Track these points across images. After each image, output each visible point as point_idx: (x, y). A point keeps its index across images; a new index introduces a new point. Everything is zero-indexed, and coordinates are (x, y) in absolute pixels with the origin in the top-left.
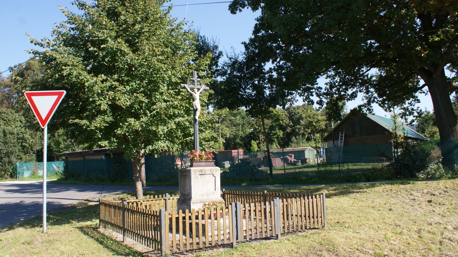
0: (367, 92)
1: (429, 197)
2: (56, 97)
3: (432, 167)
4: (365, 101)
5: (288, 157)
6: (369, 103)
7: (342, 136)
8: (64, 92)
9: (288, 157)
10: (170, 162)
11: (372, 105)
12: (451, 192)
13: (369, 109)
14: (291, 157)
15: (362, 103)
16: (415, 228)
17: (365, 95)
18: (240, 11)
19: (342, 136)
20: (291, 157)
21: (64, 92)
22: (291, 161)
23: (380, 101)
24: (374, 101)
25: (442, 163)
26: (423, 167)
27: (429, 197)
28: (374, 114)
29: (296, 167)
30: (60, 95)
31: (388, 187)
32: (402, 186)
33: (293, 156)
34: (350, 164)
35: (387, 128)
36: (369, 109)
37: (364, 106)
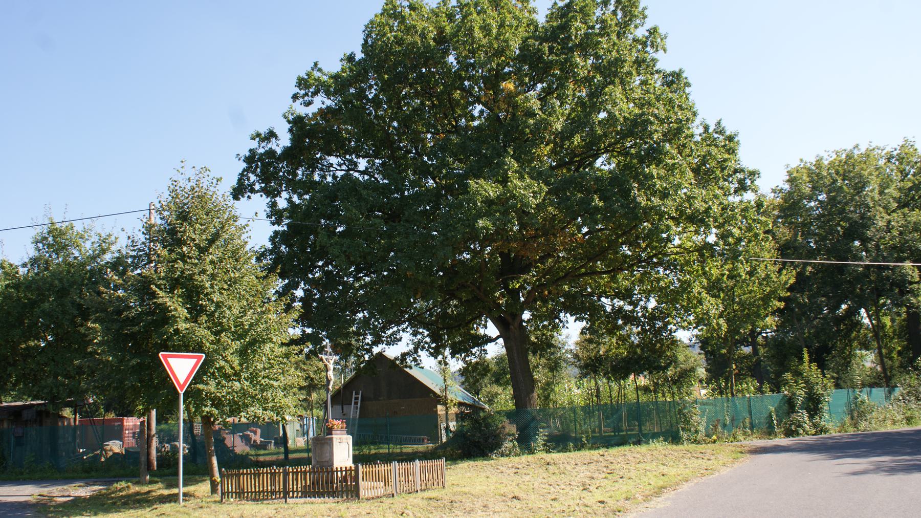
0: (415, 334)
1: (514, 470)
2: (169, 360)
3: (508, 445)
4: (411, 347)
5: (249, 433)
6: (416, 350)
7: (356, 398)
8: (163, 355)
9: (249, 433)
10: (70, 439)
11: (420, 352)
12: (533, 466)
13: (415, 360)
14: (255, 433)
15: (406, 350)
16: (514, 484)
17: (411, 337)
18: (249, 197)
19: (356, 398)
20: (255, 433)
21: (163, 355)
22: (255, 441)
23: (432, 348)
24: (423, 348)
25: (517, 440)
26: (498, 445)
27: (514, 470)
28: (422, 368)
29: (266, 452)
30: (165, 357)
31: (472, 463)
32: (486, 462)
33: (259, 431)
34: (372, 447)
35: (431, 387)
36: (415, 360)
37: (408, 354)
